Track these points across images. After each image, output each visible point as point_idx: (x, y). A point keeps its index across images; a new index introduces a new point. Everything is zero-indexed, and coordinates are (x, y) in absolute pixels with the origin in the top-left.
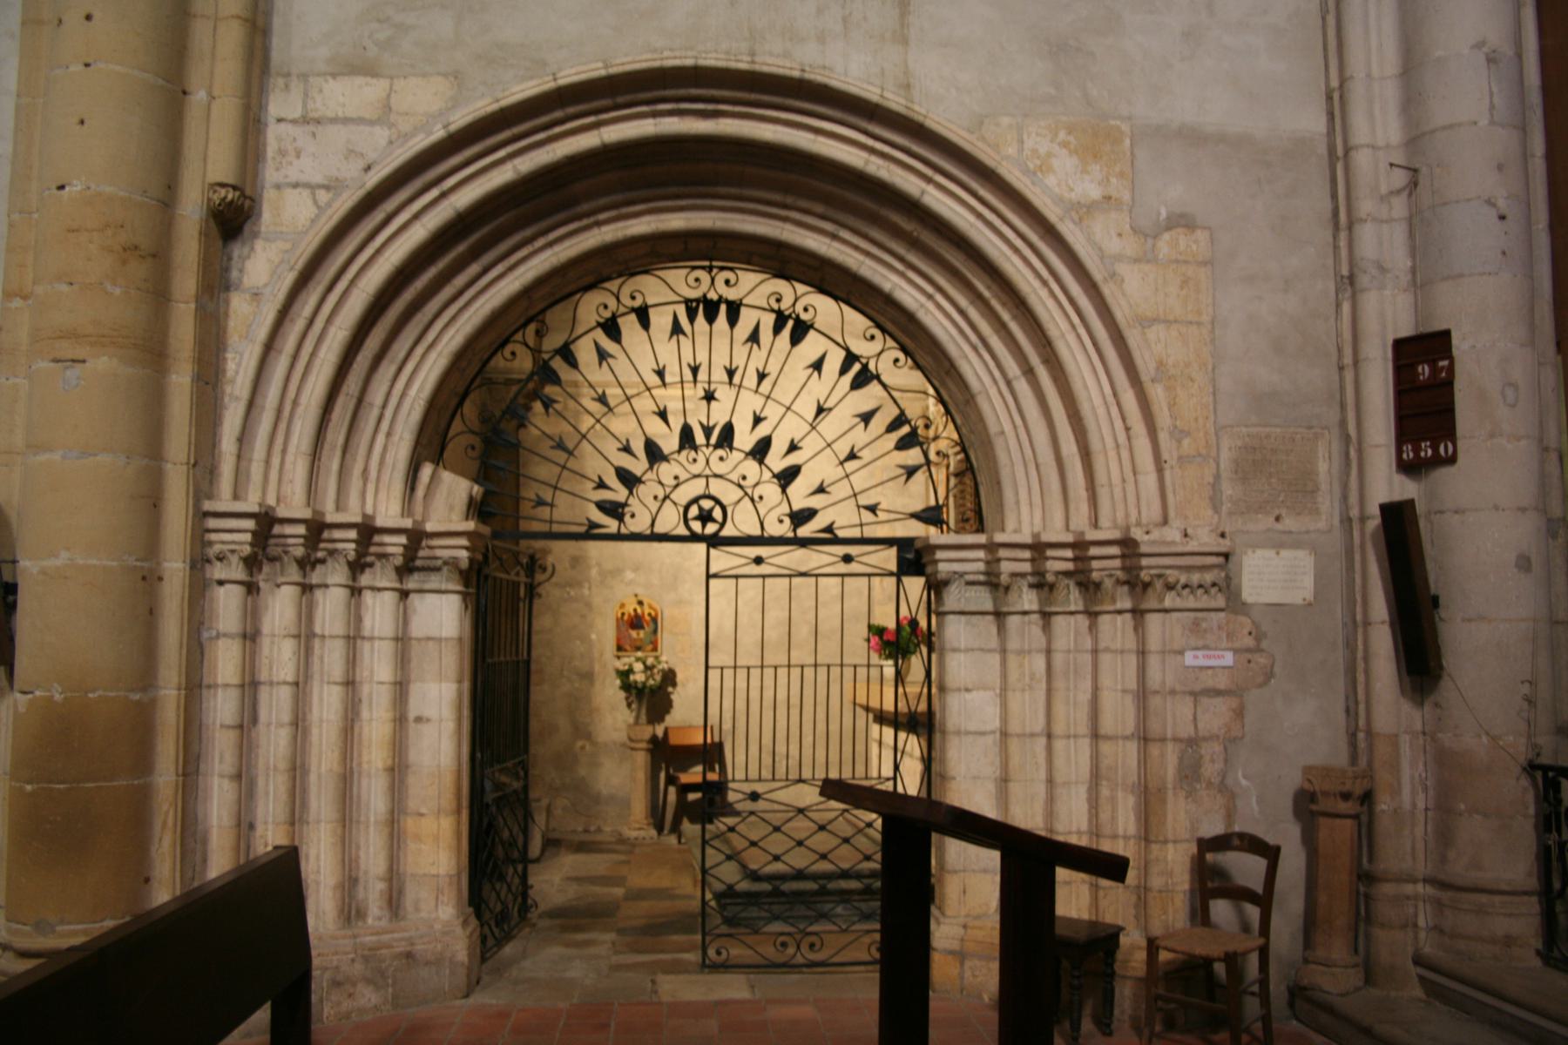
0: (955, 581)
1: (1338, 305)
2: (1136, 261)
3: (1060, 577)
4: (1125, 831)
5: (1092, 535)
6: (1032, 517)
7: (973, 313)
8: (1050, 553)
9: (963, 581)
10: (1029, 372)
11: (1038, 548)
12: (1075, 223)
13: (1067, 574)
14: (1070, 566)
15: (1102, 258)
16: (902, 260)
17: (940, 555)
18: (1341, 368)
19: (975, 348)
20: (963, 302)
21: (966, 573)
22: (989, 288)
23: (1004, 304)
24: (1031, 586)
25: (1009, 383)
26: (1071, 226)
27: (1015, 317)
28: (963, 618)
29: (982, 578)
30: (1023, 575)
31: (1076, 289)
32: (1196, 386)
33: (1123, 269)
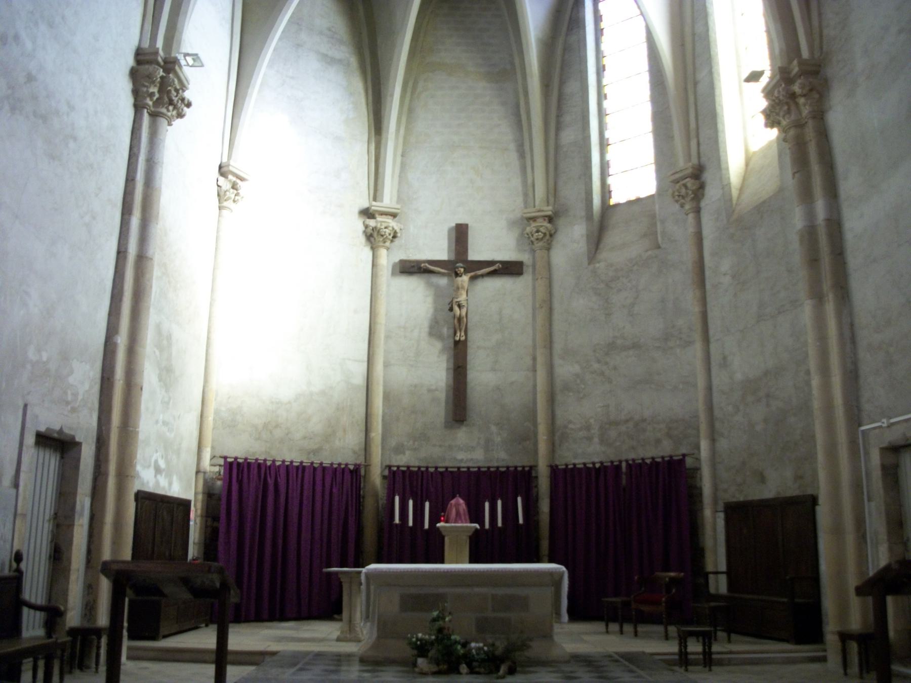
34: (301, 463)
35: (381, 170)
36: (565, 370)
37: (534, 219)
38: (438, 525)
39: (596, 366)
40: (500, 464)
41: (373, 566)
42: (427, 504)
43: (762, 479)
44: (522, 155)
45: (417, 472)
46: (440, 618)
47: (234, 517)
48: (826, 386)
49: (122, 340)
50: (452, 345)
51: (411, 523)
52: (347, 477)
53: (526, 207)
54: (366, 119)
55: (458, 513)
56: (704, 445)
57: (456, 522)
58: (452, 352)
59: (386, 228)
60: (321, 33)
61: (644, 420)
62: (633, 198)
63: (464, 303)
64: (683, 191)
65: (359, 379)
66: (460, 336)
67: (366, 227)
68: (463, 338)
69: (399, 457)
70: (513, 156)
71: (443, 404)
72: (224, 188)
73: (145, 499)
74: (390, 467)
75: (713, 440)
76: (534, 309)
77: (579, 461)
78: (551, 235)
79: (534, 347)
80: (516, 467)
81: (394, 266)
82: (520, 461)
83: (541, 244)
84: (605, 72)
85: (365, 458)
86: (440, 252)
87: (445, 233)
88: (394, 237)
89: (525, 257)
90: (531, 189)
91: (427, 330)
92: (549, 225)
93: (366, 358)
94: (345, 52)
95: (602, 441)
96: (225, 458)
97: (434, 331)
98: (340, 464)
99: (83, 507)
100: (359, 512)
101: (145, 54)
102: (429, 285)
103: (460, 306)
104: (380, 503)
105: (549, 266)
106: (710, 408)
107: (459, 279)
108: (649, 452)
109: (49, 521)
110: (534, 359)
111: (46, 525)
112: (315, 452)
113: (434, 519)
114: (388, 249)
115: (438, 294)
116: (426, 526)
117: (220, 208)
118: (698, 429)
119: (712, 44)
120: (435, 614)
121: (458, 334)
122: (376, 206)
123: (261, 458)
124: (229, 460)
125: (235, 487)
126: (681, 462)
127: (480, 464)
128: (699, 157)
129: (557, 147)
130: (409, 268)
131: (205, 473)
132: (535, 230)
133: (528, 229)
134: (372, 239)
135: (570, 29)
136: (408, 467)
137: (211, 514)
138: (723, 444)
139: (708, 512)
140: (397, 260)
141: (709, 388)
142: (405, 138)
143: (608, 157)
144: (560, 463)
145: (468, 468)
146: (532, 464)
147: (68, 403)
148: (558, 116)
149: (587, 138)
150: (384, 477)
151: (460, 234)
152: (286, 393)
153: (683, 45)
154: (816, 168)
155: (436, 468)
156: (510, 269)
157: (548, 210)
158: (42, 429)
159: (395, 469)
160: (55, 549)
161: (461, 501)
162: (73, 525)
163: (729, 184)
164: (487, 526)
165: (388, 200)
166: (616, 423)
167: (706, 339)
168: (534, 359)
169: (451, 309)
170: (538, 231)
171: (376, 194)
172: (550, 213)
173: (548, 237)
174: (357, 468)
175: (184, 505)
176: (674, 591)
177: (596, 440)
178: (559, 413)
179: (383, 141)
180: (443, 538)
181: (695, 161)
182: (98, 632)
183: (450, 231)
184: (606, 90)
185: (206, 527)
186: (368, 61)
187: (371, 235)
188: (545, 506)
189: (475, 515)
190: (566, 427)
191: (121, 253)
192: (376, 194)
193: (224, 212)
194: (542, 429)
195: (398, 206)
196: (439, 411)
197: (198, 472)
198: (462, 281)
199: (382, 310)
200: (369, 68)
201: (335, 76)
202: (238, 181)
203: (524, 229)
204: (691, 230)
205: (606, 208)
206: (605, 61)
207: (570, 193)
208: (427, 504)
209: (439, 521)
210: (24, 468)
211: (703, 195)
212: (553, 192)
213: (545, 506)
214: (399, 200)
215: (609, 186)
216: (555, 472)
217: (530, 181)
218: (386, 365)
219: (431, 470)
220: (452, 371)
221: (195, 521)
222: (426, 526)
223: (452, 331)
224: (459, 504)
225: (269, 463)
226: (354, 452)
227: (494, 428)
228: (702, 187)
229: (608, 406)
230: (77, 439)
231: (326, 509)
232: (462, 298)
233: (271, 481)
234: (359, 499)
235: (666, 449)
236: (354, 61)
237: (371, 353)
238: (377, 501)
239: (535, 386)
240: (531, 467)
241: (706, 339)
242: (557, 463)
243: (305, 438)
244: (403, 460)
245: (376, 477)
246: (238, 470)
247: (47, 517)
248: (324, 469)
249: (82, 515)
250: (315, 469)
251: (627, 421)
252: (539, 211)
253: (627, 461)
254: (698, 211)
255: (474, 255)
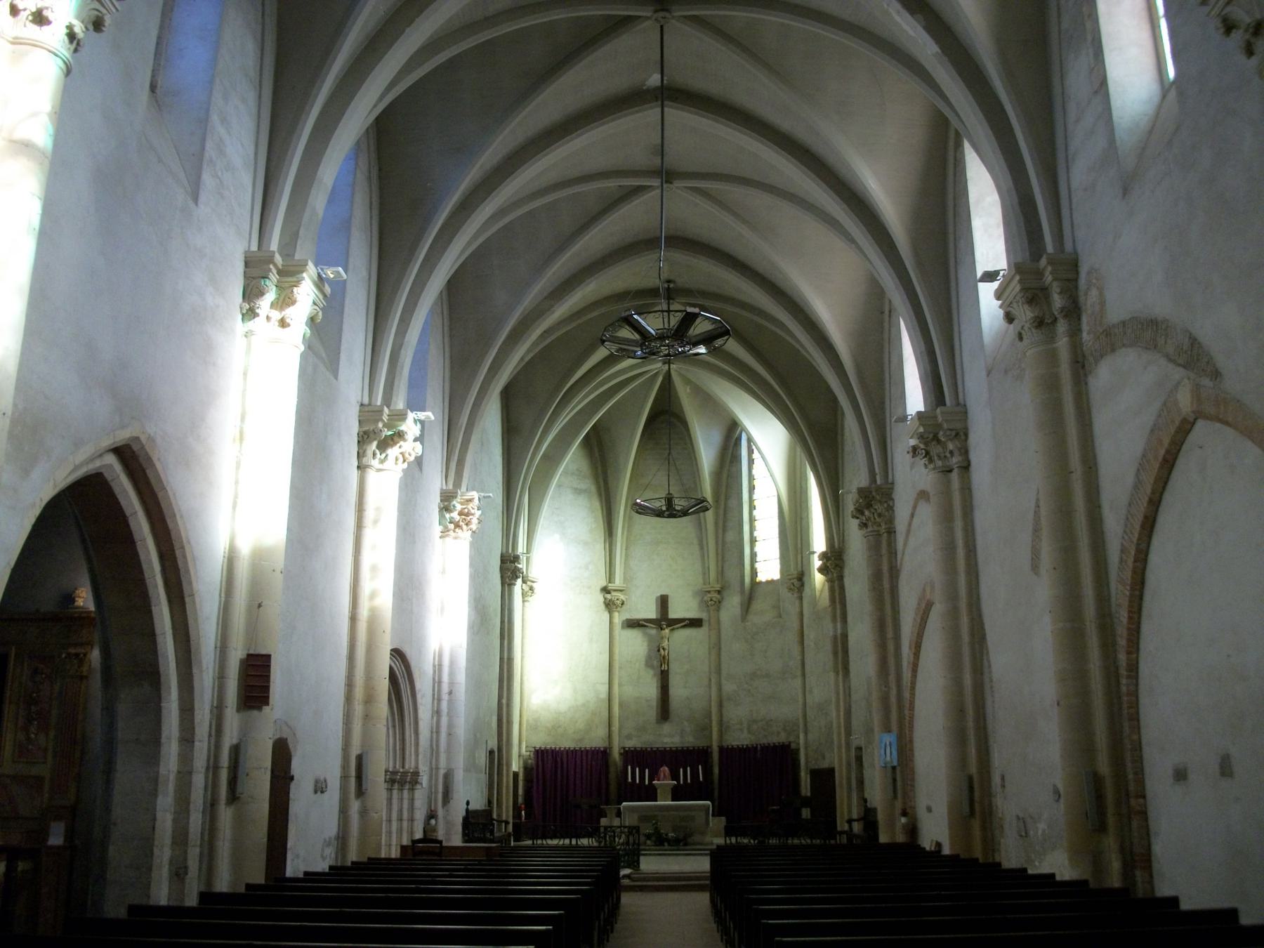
1: (432, 717)
18: (432, 732)
34: (575, 748)
35: (613, 561)
36: (729, 687)
37: (709, 592)
38: (654, 782)
39: (746, 686)
40: (689, 745)
41: (624, 803)
42: (647, 770)
43: (824, 758)
44: (702, 548)
45: (640, 751)
46: (656, 823)
47: (541, 782)
48: (838, 716)
49: (504, 701)
50: (660, 672)
51: (638, 781)
52: (600, 755)
53: (704, 584)
54: (602, 526)
55: (664, 775)
56: (802, 736)
57: (663, 780)
58: (660, 677)
59: (618, 600)
60: (573, 474)
61: (772, 720)
62: (770, 579)
63: (666, 647)
64: (792, 587)
65: (604, 695)
66: (664, 667)
67: (605, 599)
68: (666, 669)
69: (630, 741)
70: (696, 548)
71: (655, 709)
72: (526, 590)
73: (514, 772)
74: (624, 748)
75: (806, 733)
76: (709, 648)
77: (735, 743)
78: (720, 602)
79: (710, 672)
80: (699, 747)
81: (623, 624)
82: (701, 743)
83: (713, 607)
84: (755, 491)
85: (609, 743)
86: (651, 612)
87: (655, 598)
88: (622, 604)
89: (703, 615)
90: (707, 571)
91: (644, 663)
92: (718, 596)
93: (607, 682)
94: (588, 484)
95: (749, 732)
96: (535, 748)
97: (648, 664)
98: (595, 748)
100: (607, 773)
101: (504, 557)
102: (645, 634)
103: (664, 649)
104: (619, 769)
105: (718, 622)
106: (805, 716)
107: (663, 632)
108: (775, 739)
110: (710, 680)
112: (581, 740)
113: (651, 779)
114: (619, 612)
115: (650, 640)
116: (647, 783)
117: (524, 601)
118: (798, 726)
119: (809, 499)
120: (654, 822)
121: (663, 666)
122: (611, 586)
125: (540, 763)
126: (789, 745)
127: (677, 745)
128: (802, 567)
129: (724, 542)
130: (632, 624)
131: (523, 756)
132: (709, 599)
133: (705, 598)
134: (609, 607)
135: (731, 462)
136: (635, 748)
138: (810, 736)
139: (803, 774)
140: (624, 618)
141: (805, 704)
142: (627, 539)
143: (757, 549)
144: (725, 744)
145: (671, 748)
146: (709, 745)
148: (725, 522)
149: (742, 539)
150: (621, 754)
151: (663, 602)
152: (563, 707)
153: (795, 492)
154: (838, 606)
155: (652, 748)
156: (695, 623)
157: (718, 587)
159: (627, 749)
161: (666, 769)
163: (815, 588)
164: (682, 782)
165: (618, 582)
166: (755, 721)
167: (804, 675)
168: (710, 680)
169: (659, 651)
170: (711, 600)
171: (611, 578)
172: (718, 589)
173: (717, 603)
174: (605, 749)
177: (745, 731)
179: (614, 542)
180: (656, 789)
181: (800, 569)
182: (509, 834)
183: (657, 598)
184: (756, 503)
186: (603, 489)
187: (609, 604)
188: (716, 770)
189: (675, 776)
190: (728, 722)
191: (501, 659)
192: (611, 578)
193: (526, 603)
194: (714, 724)
195: (625, 585)
196: (652, 713)
198: (661, 303)
199: (617, 650)
200: (603, 493)
201: (582, 501)
202: (532, 584)
203: (703, 598)
204: (798, 610)
205: (755, 584)
206: (755, 483)
207: (731, 574)
208: (647, 770)
209: (654, 780)
211: (803, 590)
212: (721, 573)
213: (716, 770)
214: (625, 579)
215: (756, 569)
216: (722, 750)
217: (707, 565)
218: (620, 685)
219: (649, 749)
220: (660, 689)
222: (647, 783)
223: (659, 664)
224: (665, 770)
225: (557, 749)
226: (603, 739)
227: (686, 723)
228: (803, 585)
229: (751, 711)
232: (665, 644)
233: (559, 759)
234: (607, 766)
235: (782, 738)
236: (593, 489)
238: (617, 768)
239: (711, 697)
240: (708, 747)
241: (804, 675)
242: (724, 744)
243: (574, 733)
244: (631, 744)
245: (616, 754)
248: (587, 751)
250: (582, 751)
251: (762, 720)
252: (712, 587)
253: (760, 745)
254: (801, 598)
255: (673, 614)
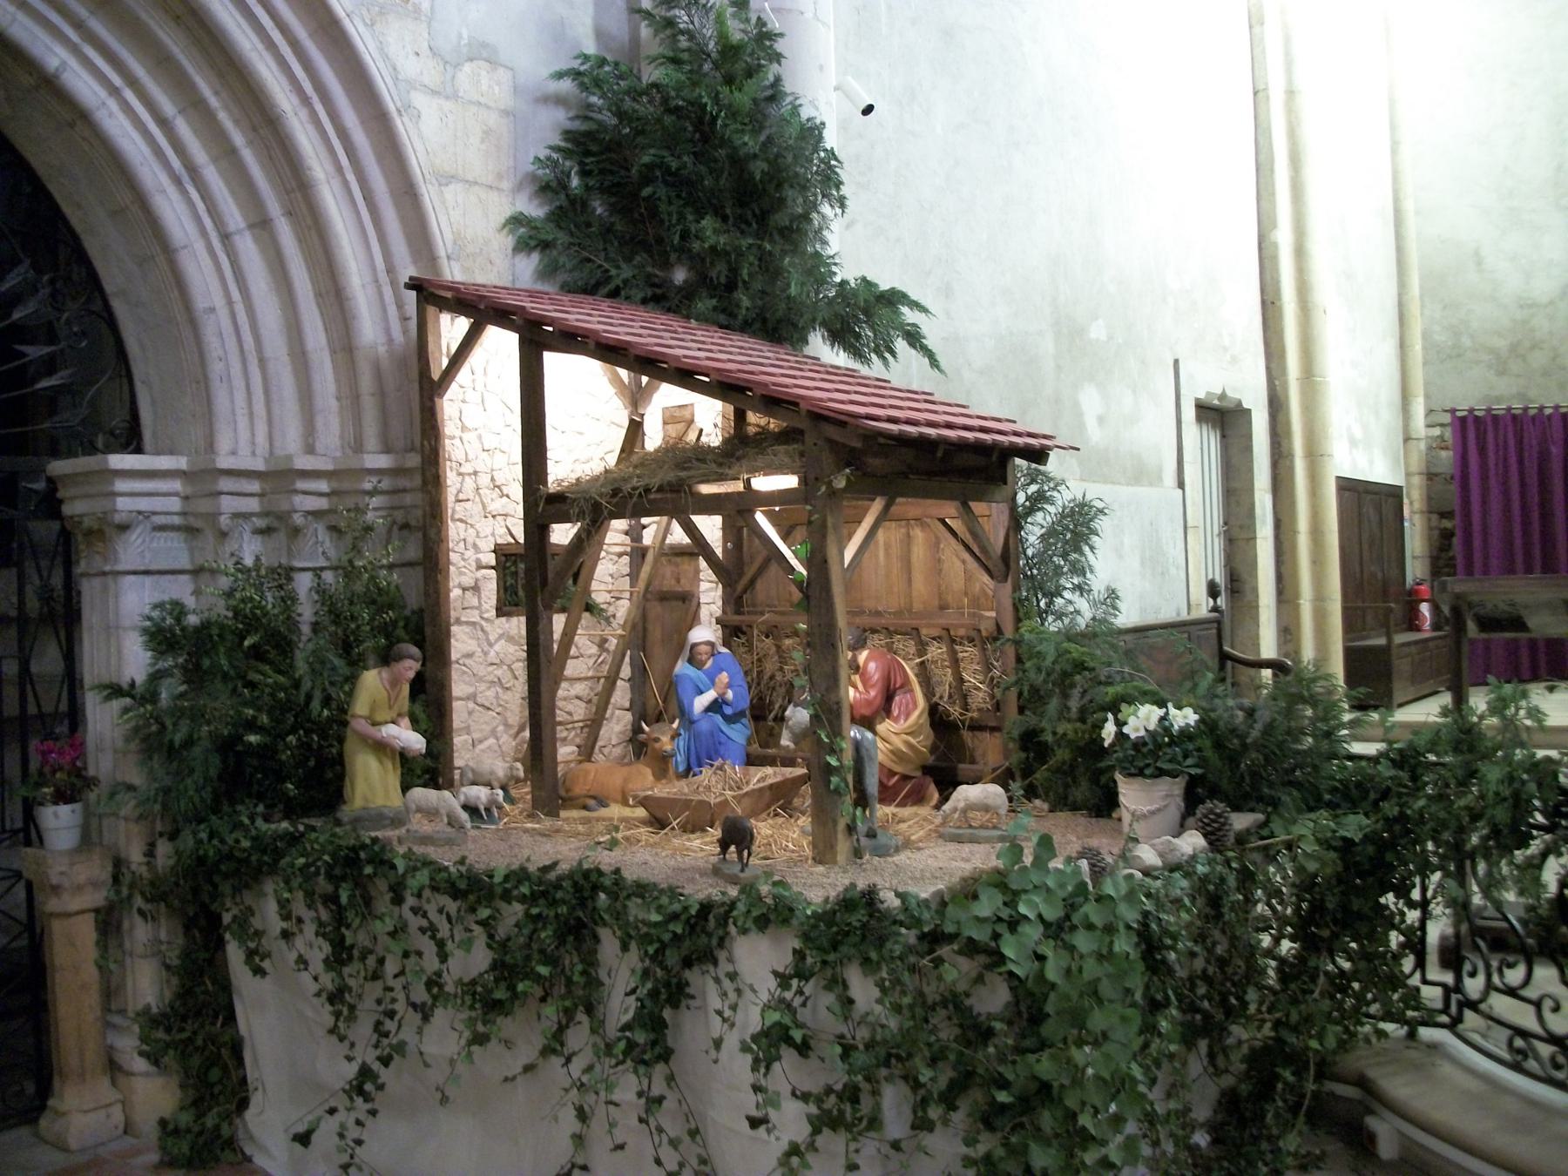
0: (140, 522)
2: (435, 93)
3: (310, 518)
4: (95, 884)
5: (304, 462)
6: (253, 435)
7: (183, 128)
8: (301, 485)
9: (149, 526)
10: (261, 225)
11: (280, 477)
12: (366, 24)
13: (316, 514)
14: (322, 504)
15: (396, 79)
16: (78, 25)
17: (121, 485)
19: (178, 181)
20: (168, 108)
21: (155, 513)
22: (216, 93)
23: (237, 122)
24: (259, 532)
25: (226, 237)
26: (361, 28)
27: (250, 143)
28: (148, 580)
29: (177, 520)
30: (245, 516)
31: (350, 118)
32: (495, 270)
33: (419, 100)
73: (1350, 489)
96: (1453, 411)
99: (1263, 508)
109: (1219, 535)
111: (1216, 540)
123: (1517, 405)
124: (1459, 414)
137: (1436, 510)
147: (1225, 349)
158: (1202, 396)
160: (1231, 575)
162: (1255, 538)
175: (1393, 495)
176: (84, 344)
178: (277, 444)
185: (1431, 529)
197: (1407, 439)
210: (1187, 457)
221: (1411, 520)
230: (1245, 406)
231: (1533, 479)
237: (1268, 277)
246: (1477, 429)
247: (1216, 531)
249: (1264, 522)
